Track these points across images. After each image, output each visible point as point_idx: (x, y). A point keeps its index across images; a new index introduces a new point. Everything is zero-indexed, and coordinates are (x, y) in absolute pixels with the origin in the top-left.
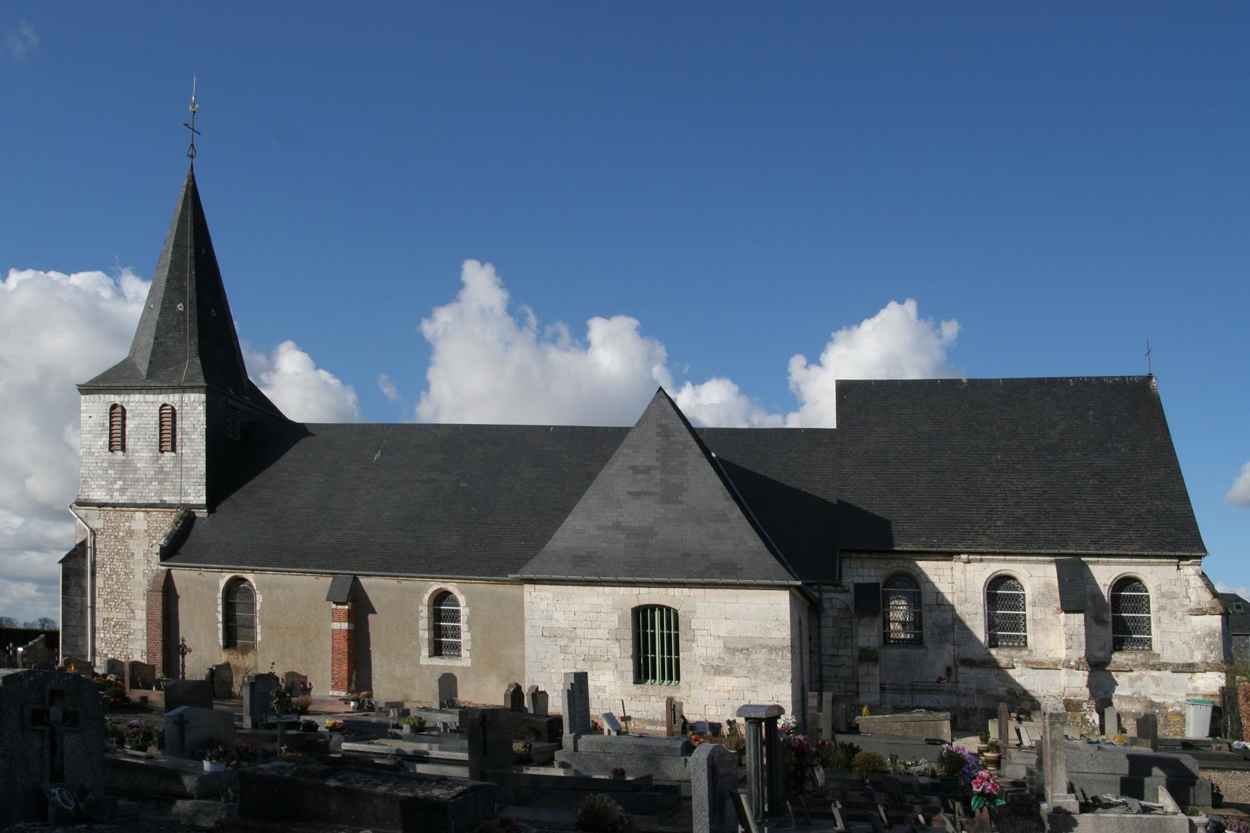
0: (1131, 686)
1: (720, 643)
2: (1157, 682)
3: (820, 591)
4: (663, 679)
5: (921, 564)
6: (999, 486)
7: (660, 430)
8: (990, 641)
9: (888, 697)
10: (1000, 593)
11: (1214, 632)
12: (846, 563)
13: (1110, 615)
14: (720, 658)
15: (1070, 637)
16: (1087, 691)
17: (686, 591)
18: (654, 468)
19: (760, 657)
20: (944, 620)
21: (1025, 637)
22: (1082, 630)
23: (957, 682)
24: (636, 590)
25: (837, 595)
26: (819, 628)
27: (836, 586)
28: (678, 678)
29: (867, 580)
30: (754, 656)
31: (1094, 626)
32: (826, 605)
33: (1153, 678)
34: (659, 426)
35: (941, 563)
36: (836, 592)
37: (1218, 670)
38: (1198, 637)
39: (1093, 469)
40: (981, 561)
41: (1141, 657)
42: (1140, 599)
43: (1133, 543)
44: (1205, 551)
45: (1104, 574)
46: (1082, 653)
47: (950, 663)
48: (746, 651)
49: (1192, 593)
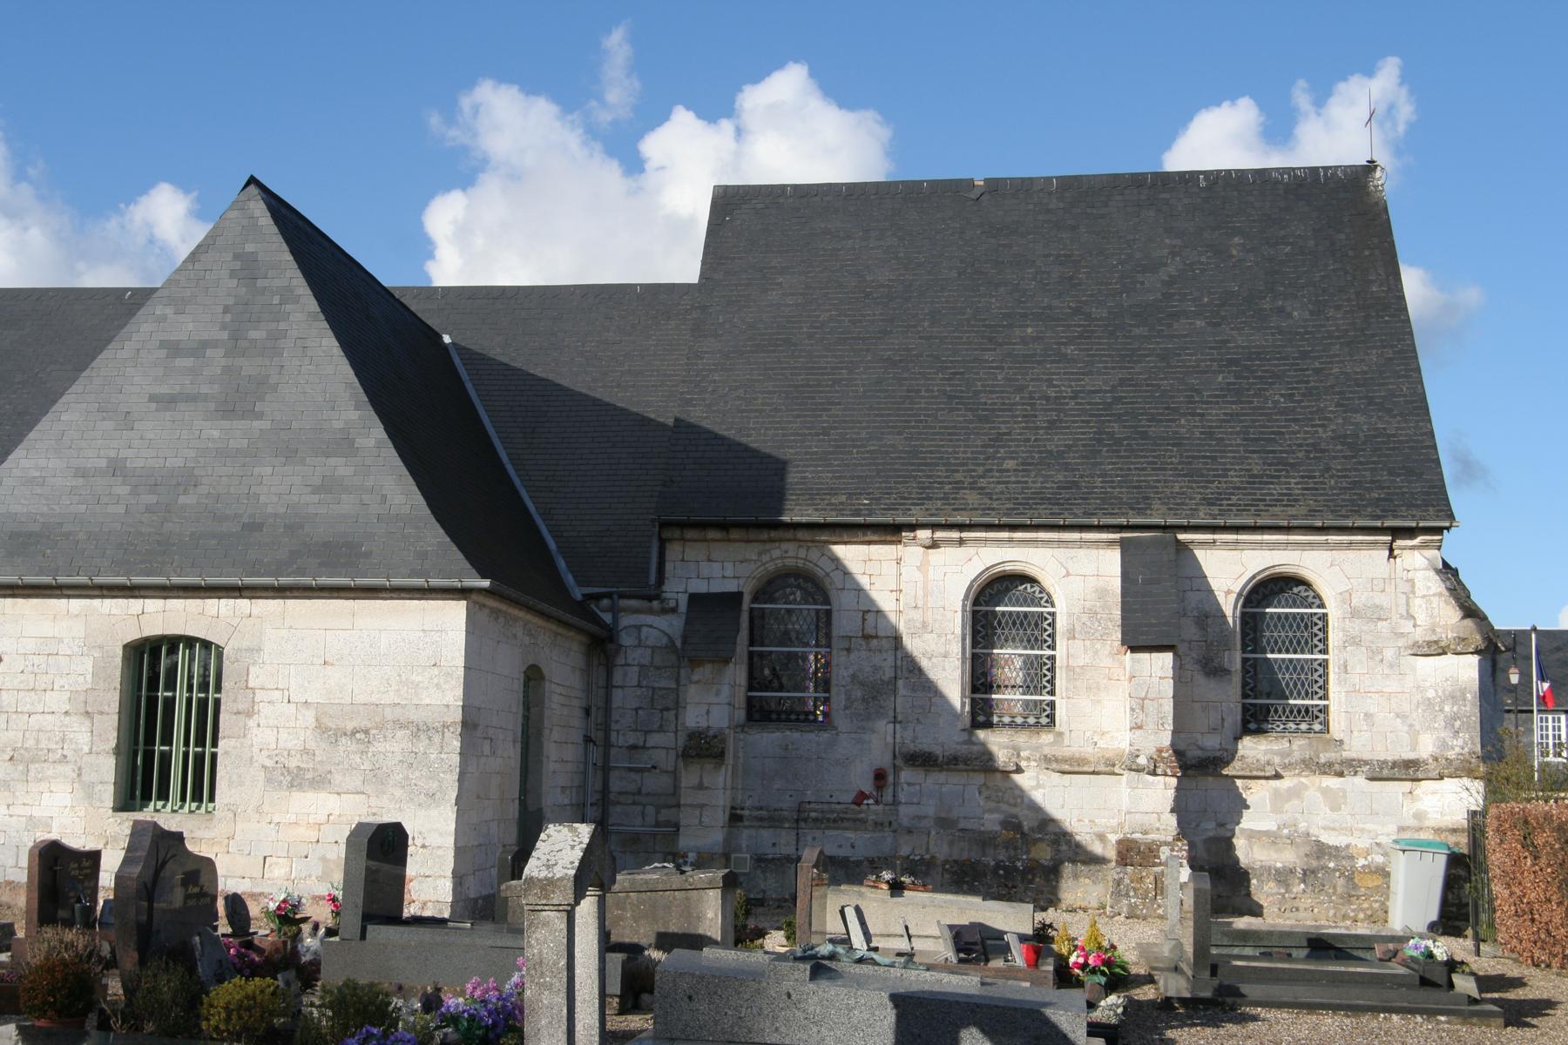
0: (1277, 810)
1: (309, 717)
2: (1335, 801)
3: (614, 610)
4: (183, 799)
5: (840, 550)
6: (1020, 389)
7: (238, 265)
8: (973, 713)
9: (745, 836)
10: (997, 608)
11: (1463, 692)
12: (673, 551)
13: (1238, 656)
14: (305, 751)
15: (1140, 703)
16: (1172, 821)
17: (243, 604)
18: (214, 344)
19: (394, 747)
20: (876, 669)
21: (1052, 705)
22: (1168, 688)
23: (895, 802)
24: (135, 605)
25: (650, 619)
26: (609, 687)
27: (650, 599)
28: (212, 799)
29: (717, 587)
30: (379, 746)
31: (1200, 679)
32: (626, 640)
33: (1325, 792)
34: (236, 257)
35: (876, 550)
36: (651, 611)
37: (1471, 773)
38: (1429, 703)
39: (1252, 362)
40: (961, 542)
41: (1299, 746)
42: (1306, 623)
43: (1293, 502)
44: (1451, 517)
45: (1228, 568)
46: (1166, 739)
47: (883, 759)
48: (361, 735)
49: (1418, 606)
